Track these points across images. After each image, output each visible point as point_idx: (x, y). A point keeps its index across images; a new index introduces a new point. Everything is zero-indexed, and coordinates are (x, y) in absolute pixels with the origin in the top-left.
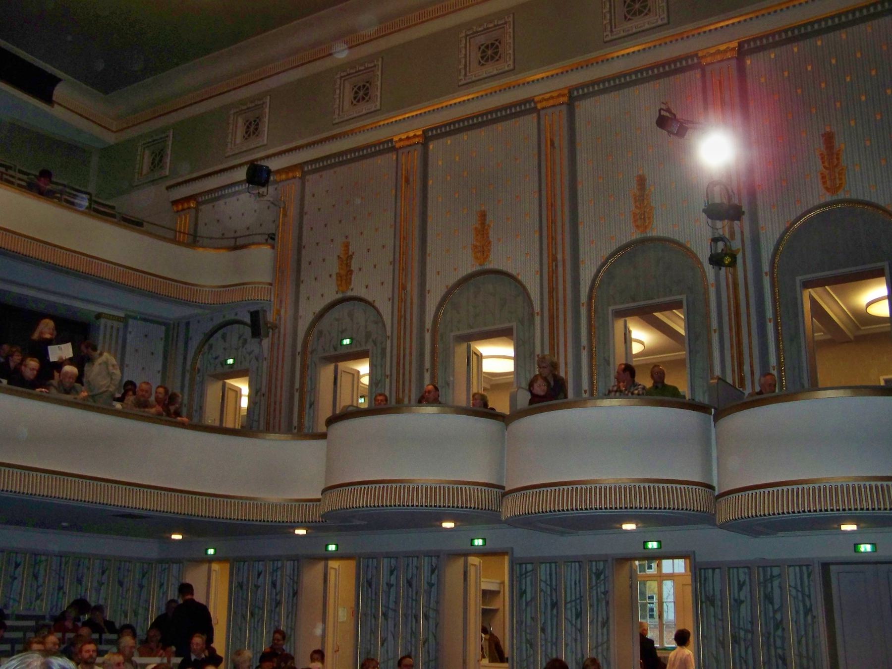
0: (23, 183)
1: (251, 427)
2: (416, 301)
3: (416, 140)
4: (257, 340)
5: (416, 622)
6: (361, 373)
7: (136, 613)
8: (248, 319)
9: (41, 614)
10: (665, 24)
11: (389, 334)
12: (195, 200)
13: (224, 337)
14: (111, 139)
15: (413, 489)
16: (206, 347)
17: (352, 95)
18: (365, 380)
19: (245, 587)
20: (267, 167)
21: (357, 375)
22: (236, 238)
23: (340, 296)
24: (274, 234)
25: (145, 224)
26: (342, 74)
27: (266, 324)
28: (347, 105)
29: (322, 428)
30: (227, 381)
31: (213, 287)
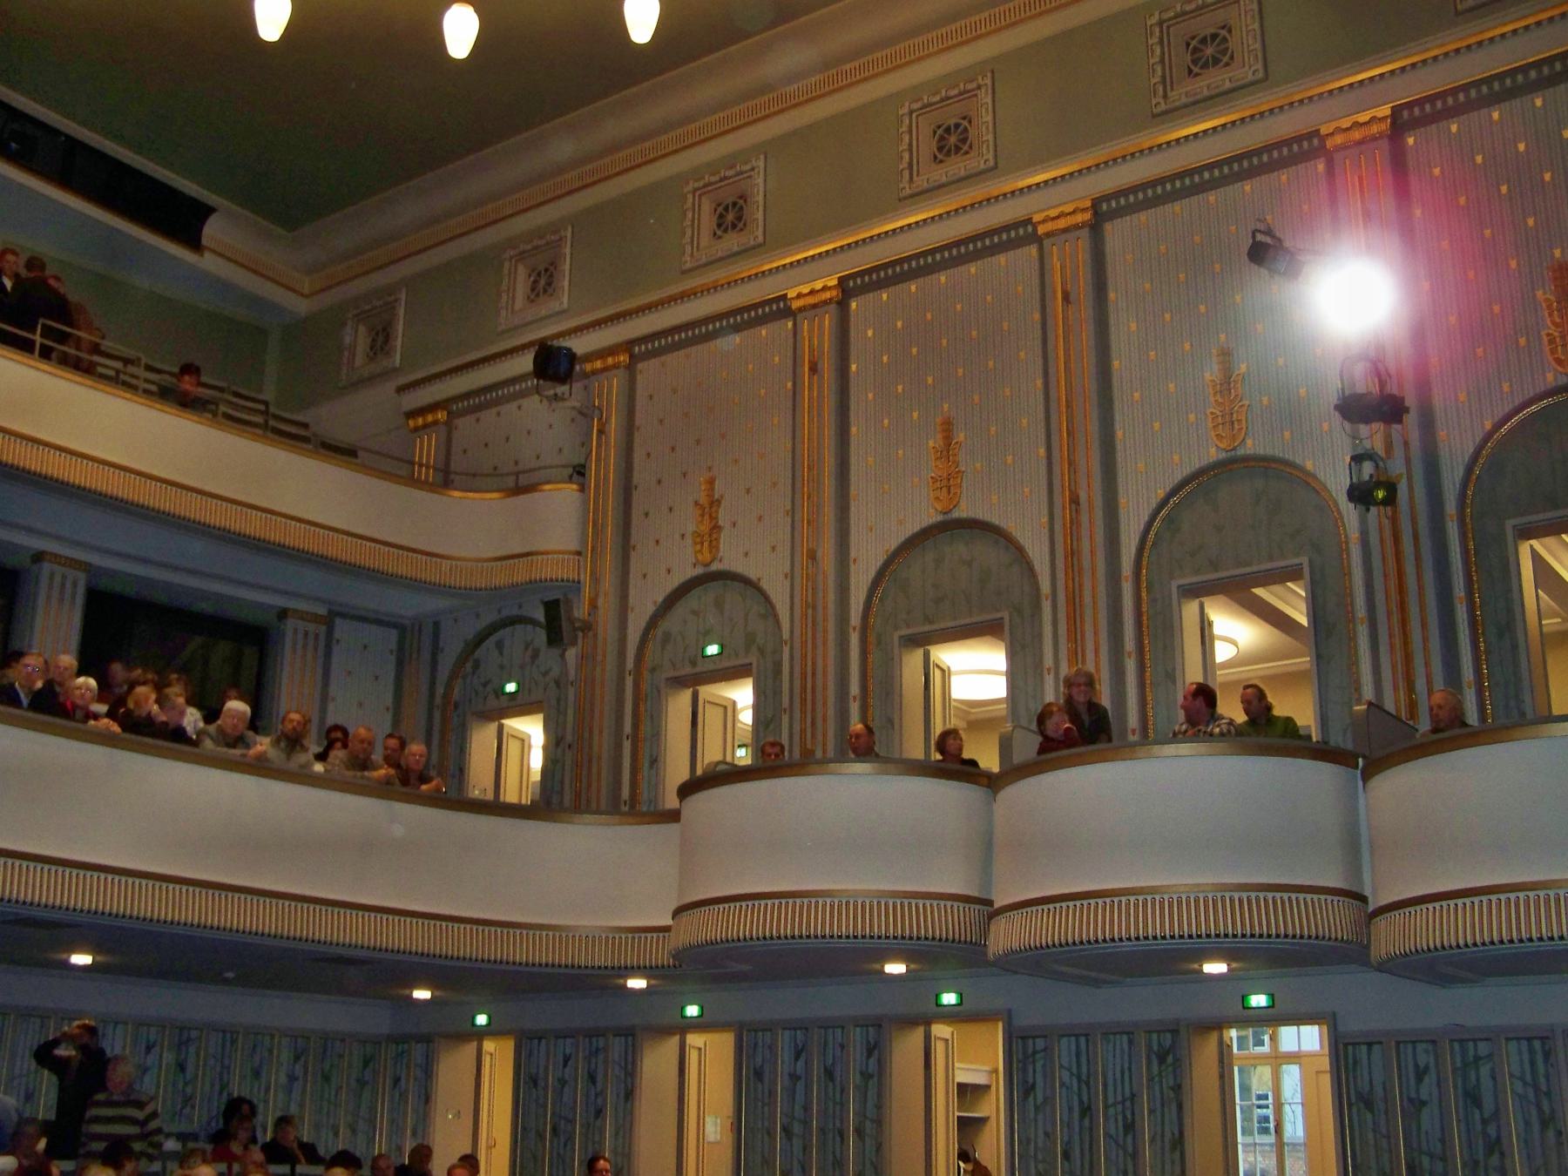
0: (154, 388)
3: (828, 295)
4: (555, 652)
6: (739, 706)
8: (540, 615)
10: (760, 245)
15: (832, 907)
16: (469, 665)
17: (715, 219)
18: (746, 717)
19: (541, 1083)
20: (569, 350)
21: (729, 709)
22: (517, 474)
23: (700, 570)
24: (583, 466)
25: (360, 453)
28: (705, 241)
29: (672, 801)
30: (506, 722)
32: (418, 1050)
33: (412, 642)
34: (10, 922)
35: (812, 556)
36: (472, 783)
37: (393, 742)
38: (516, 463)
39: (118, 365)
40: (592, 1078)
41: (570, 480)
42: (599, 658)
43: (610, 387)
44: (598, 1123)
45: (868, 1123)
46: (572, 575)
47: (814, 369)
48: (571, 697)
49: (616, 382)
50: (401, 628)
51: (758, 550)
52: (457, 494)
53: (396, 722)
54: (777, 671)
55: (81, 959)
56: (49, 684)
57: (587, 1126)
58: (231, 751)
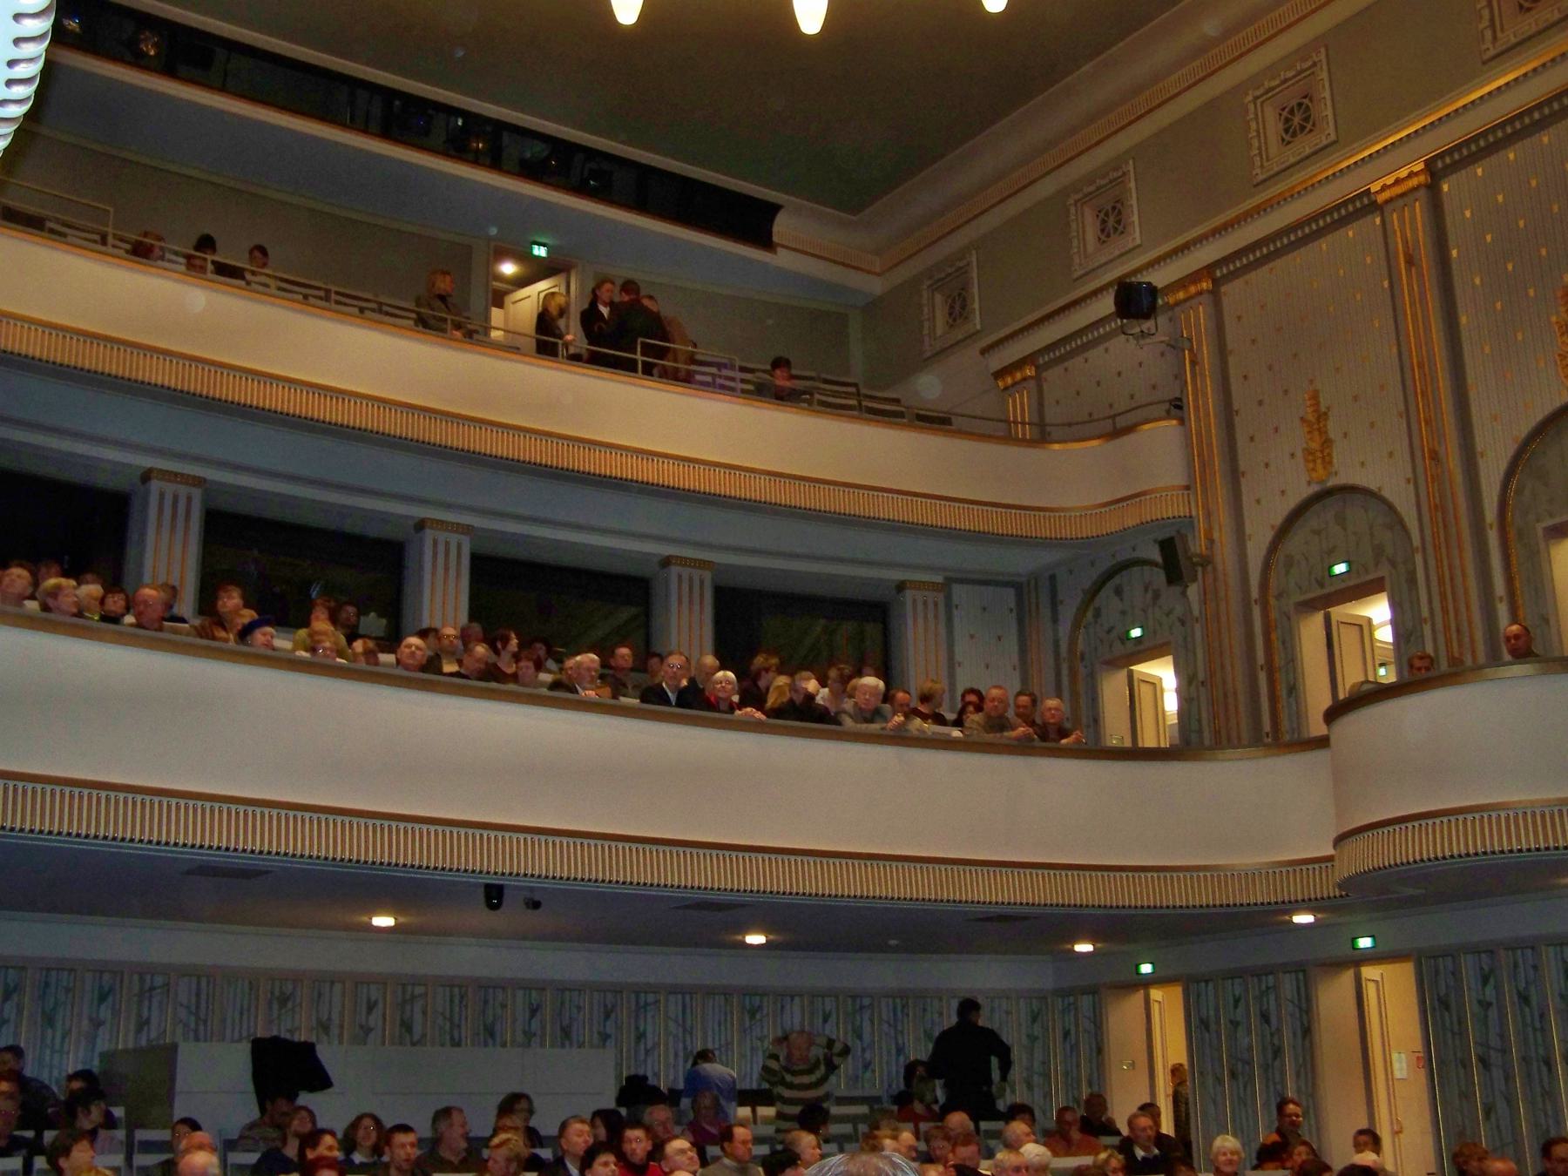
0: (750, 387)
1: (1189, 744)
2: (1459, 478)
3: (1414, 182)
4: (1177, 589)
5: (1550, 1070)
6: (1375, 622)
7: (1030, 1086)
8: (1155, 555)
9: (874, 1093)
10: (1335, 142)
11: (1416, 542)
12: (1033, 364)
13: (1118, 592)
14: (876, 286)
15: (1507, 818)
16: (1090, 614)
17: (1281, 126)
18: (1385, 635)
19: (1213, 1027)
20: (1149, 284)
21: (1364, 628)
22: (1113, 417)
23: (1315, 488)
24: (1180, 400)
25: (954, 419)
26: (1258, 93)
27: (1190, 558)
28: (1273, 150)
29: (1317, 728)
30: (1138, 668)
31: (1086, 508)
32: (1086, 1002)
33: (1028, 597)
34: (687, 907)
35: (1434, 456)
36: (1108, 732)
37: (1024, 699)
38: (1132, 397)
39: (714, 370)
40: (1265, 1017)
41: (1168, 416)
42: (1222, 594)
43: (1197, 318)
44: (1277, 1063)
45: (1036, 1078)
46: (1183, 511)
47: (1410, 262)
48: (1198, 634)
49: (1201, 314)
50: (1018, 588)
51: (1376, 462)
52: (1056, 447)
53: (1025, 679)
54: (1412, 580)
55: (755, 939)
56: (692, 681)
57: (1266, 1068)
58: (872, 725)
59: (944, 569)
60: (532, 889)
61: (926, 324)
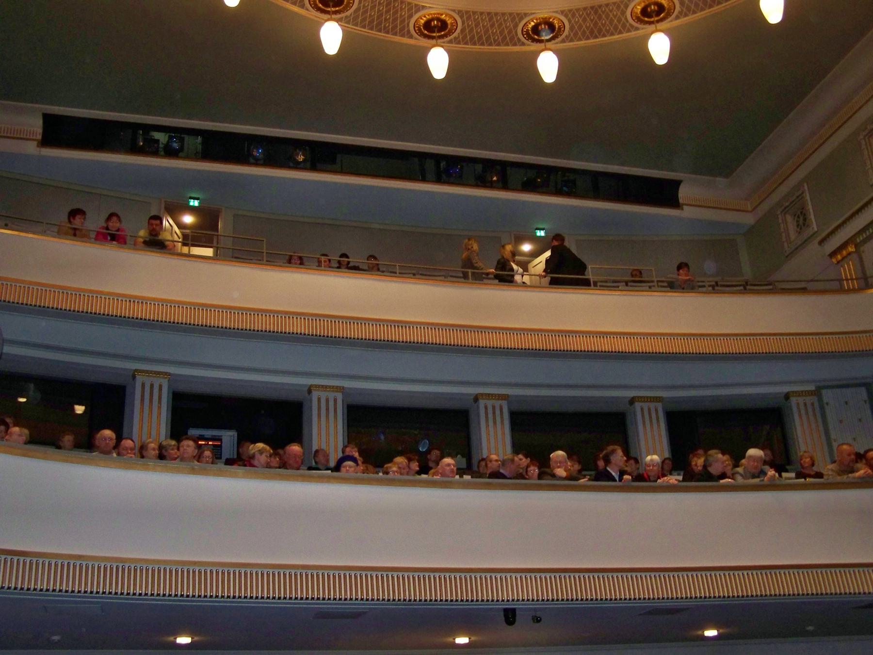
14: (749, 219)
55: (711, 633)
59: (814, 381)
60: (535, 610)
61: (784, 235)
